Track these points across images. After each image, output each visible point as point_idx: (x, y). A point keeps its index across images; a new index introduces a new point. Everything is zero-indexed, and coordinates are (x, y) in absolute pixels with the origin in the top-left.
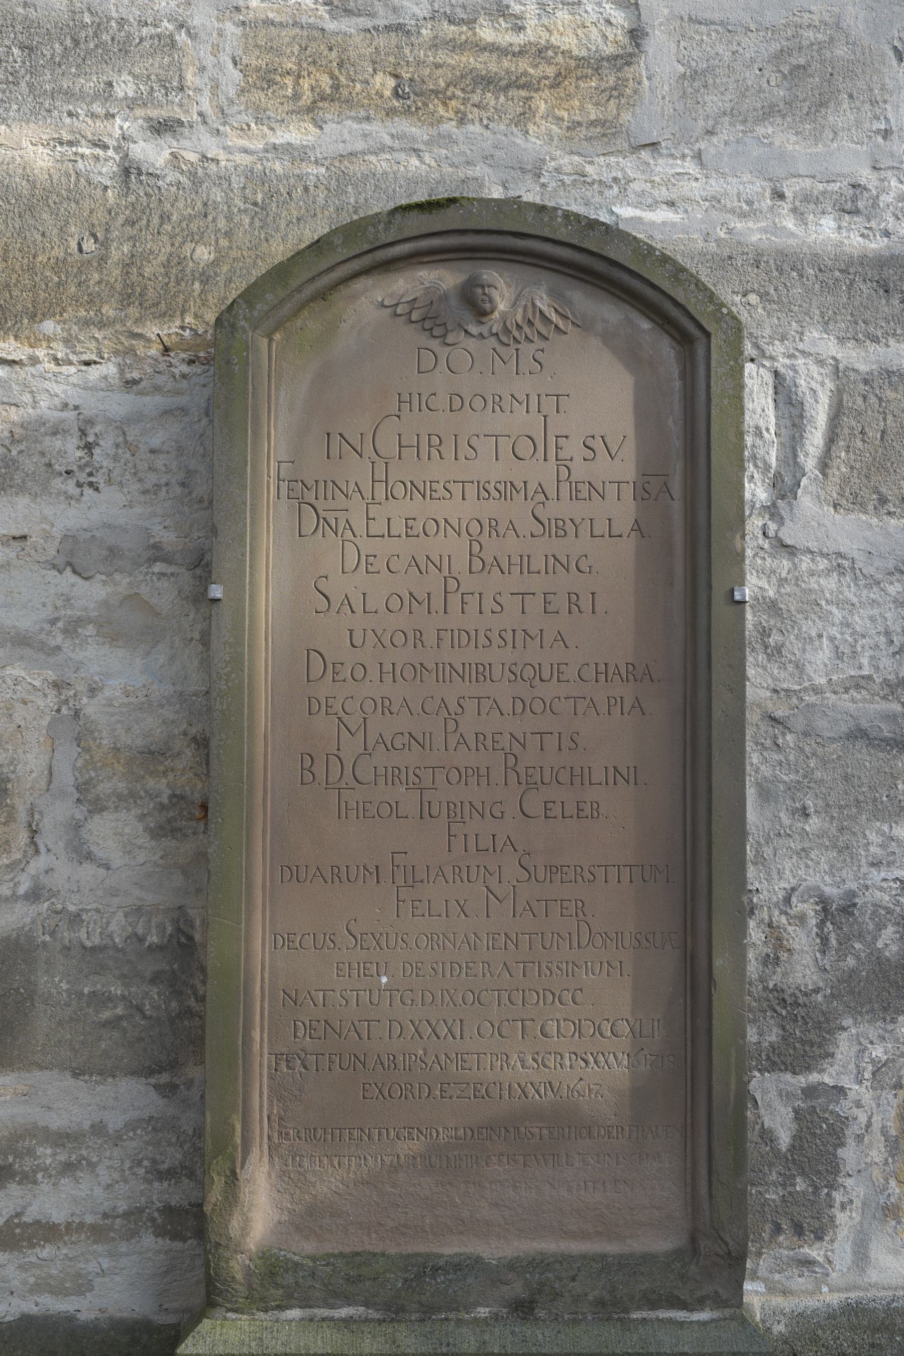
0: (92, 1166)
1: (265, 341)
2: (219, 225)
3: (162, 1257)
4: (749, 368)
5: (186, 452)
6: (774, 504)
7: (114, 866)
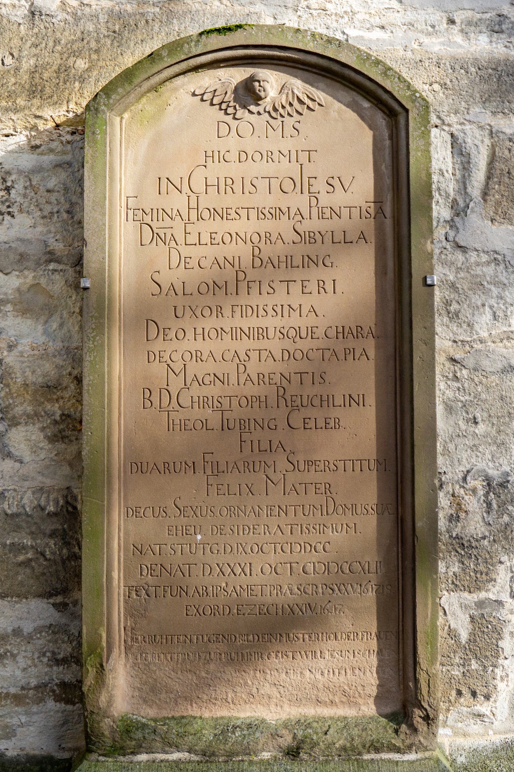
0: (14, 656)
1: (118, 119)
2: (91, 46)
3: (60, 714)
4: (434, 132)
5: (70, 191)
6: (452, 220)
7: (25, 461)
